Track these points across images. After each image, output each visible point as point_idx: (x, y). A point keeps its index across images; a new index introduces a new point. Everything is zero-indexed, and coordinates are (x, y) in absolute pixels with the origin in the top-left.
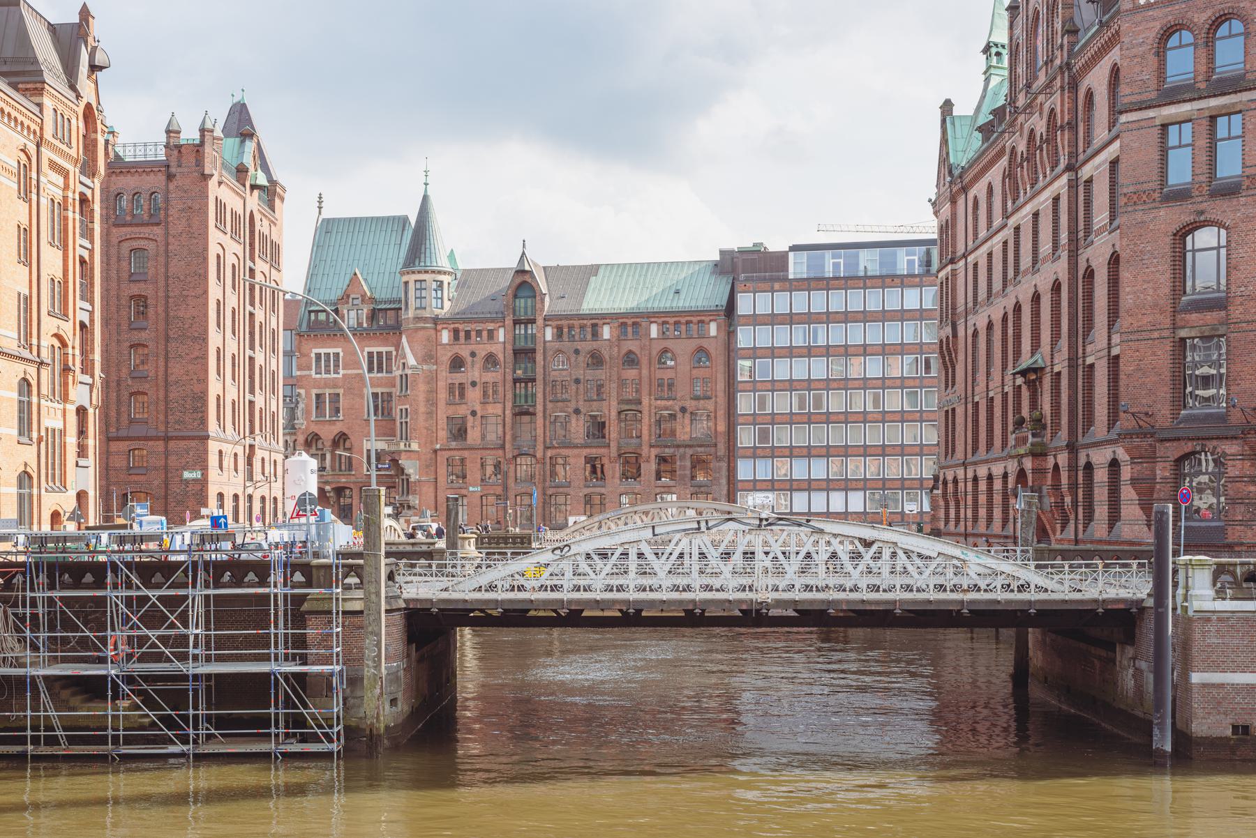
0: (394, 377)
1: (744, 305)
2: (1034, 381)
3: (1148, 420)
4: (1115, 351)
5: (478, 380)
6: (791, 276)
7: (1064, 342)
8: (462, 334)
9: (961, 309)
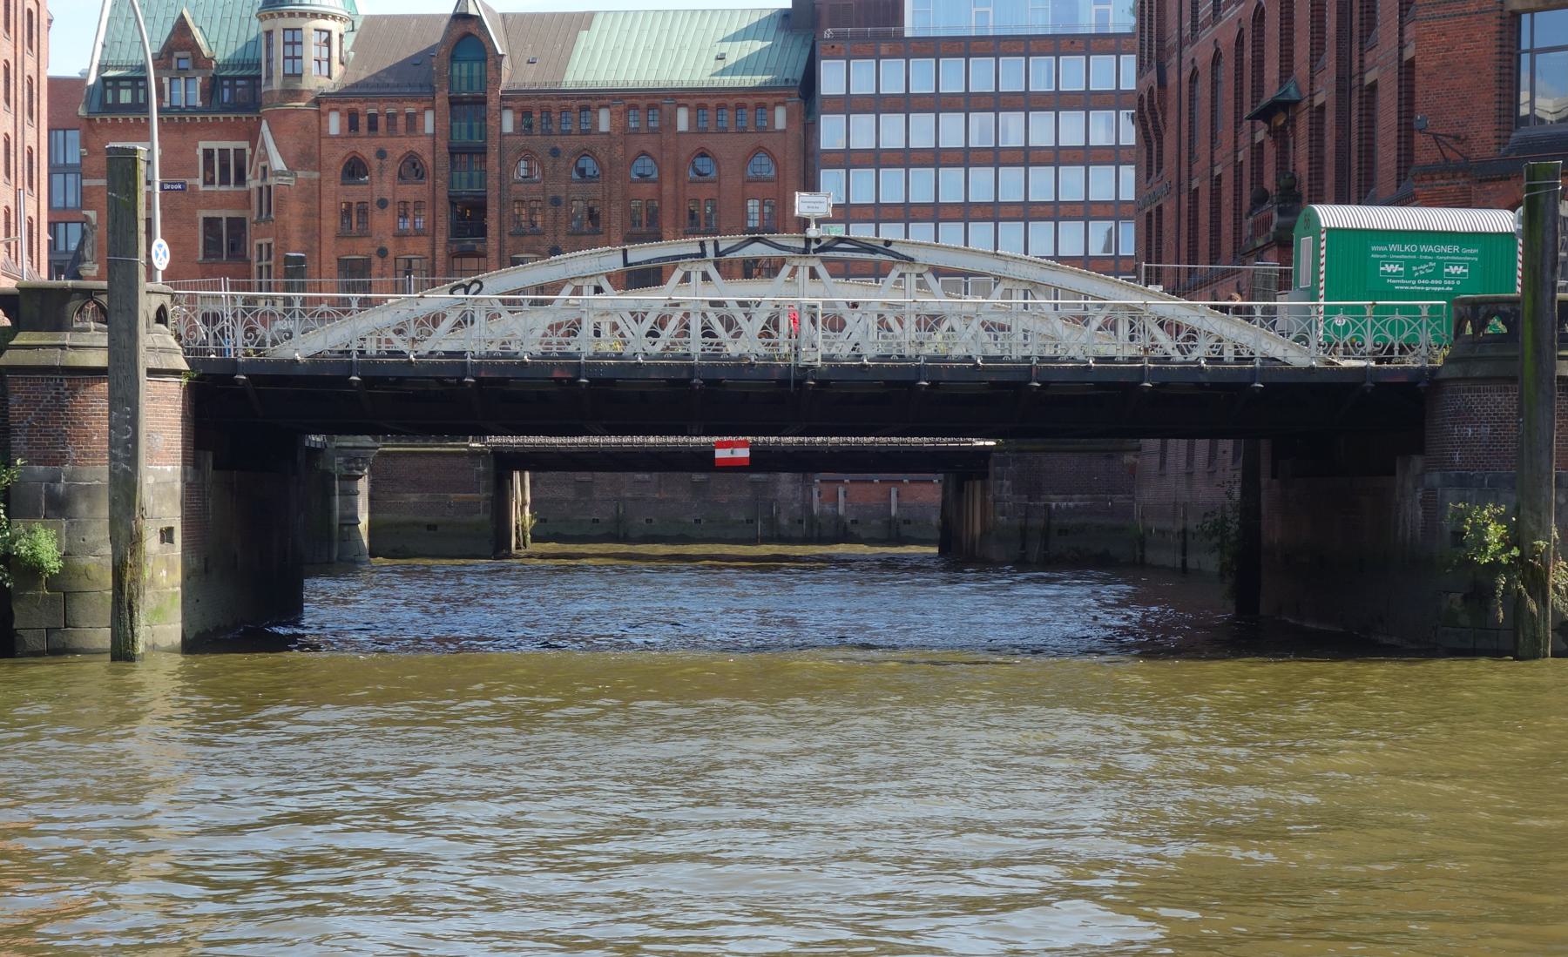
0: (249, 193)
1: (831, 78)
2: (1283, 128)
3: (1459, 148)
4: (1409, 53)
5: (389, 198)
6: (908, 34)
7: (1330, 57)
8: (363, 121)
9: (1172, 40)
